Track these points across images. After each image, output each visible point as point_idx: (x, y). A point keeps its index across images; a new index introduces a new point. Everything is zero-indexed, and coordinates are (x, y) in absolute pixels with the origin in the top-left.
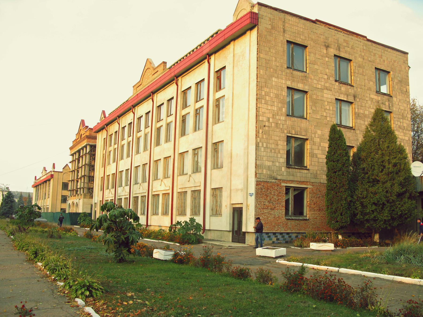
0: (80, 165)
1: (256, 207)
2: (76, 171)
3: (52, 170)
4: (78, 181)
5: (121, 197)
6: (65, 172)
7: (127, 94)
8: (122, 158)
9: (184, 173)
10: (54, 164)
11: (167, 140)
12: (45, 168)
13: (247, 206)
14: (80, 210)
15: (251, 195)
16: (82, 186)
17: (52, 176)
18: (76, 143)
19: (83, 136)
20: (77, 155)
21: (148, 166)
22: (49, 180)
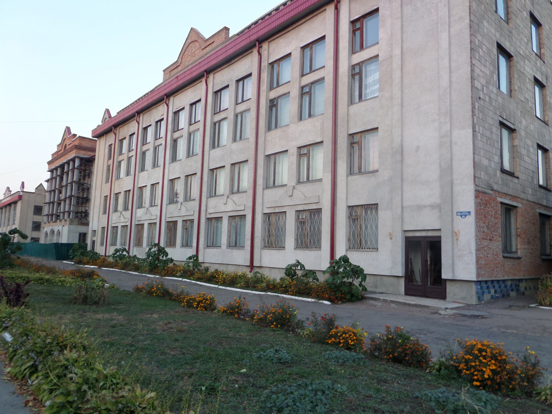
0: (64, 183)
1: (476, 236)
2: (57, 191)
3: (20, 190)
4: (59, 204)
5: (142, 222)
6: (38, 192)
7: (152, 79)
8: (143, 169)
9: (192, 199)
10: (23, 183)
11: (155, 165)
12: (8, 188)
13: (455, 235)
14: (64, 240)
15: (464, 215)
16: (66, 210)
17: (20, 197)
18: (56, 156)
19: (68, 147)
20: (58, 170)
21: (197, 178)
22: (15, 203)
